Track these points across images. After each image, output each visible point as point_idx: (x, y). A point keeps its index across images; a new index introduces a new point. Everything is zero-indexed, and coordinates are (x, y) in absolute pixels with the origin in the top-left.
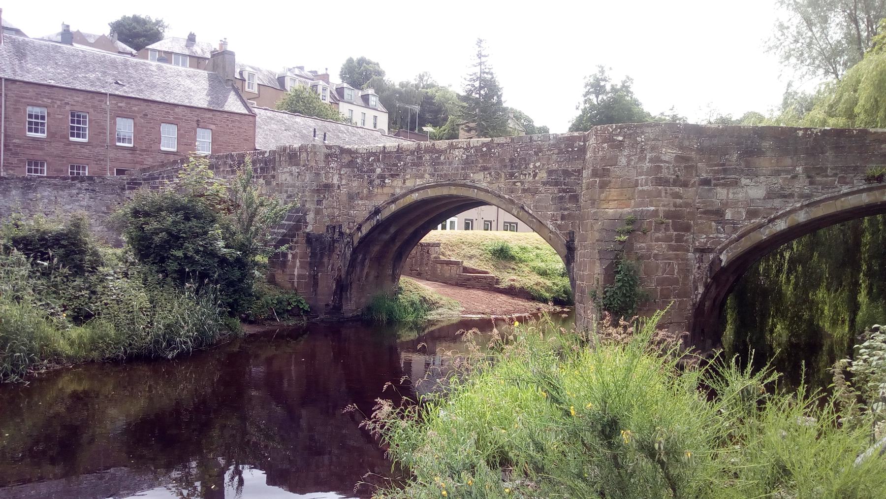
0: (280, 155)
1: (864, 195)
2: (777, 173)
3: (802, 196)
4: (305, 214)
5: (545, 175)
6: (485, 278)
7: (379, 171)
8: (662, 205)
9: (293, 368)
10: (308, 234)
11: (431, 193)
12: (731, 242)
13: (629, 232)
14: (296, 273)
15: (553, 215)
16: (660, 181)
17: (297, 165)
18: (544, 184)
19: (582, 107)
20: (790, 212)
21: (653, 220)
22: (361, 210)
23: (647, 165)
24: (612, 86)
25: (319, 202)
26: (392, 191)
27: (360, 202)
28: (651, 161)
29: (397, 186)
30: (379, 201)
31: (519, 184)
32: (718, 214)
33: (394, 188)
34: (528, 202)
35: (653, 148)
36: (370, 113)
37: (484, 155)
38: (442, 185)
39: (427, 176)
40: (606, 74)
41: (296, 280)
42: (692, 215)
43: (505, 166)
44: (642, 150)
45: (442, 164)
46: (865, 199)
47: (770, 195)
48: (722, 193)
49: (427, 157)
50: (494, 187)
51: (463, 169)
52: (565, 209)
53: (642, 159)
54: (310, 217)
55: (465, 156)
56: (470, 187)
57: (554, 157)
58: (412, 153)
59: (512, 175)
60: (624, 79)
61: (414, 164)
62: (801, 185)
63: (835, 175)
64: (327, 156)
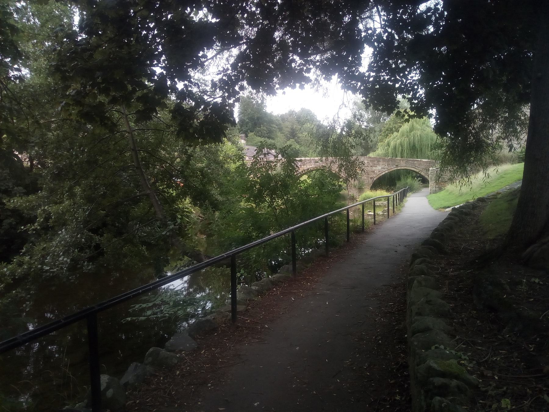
32: (374, 172)
62: (387, 167)
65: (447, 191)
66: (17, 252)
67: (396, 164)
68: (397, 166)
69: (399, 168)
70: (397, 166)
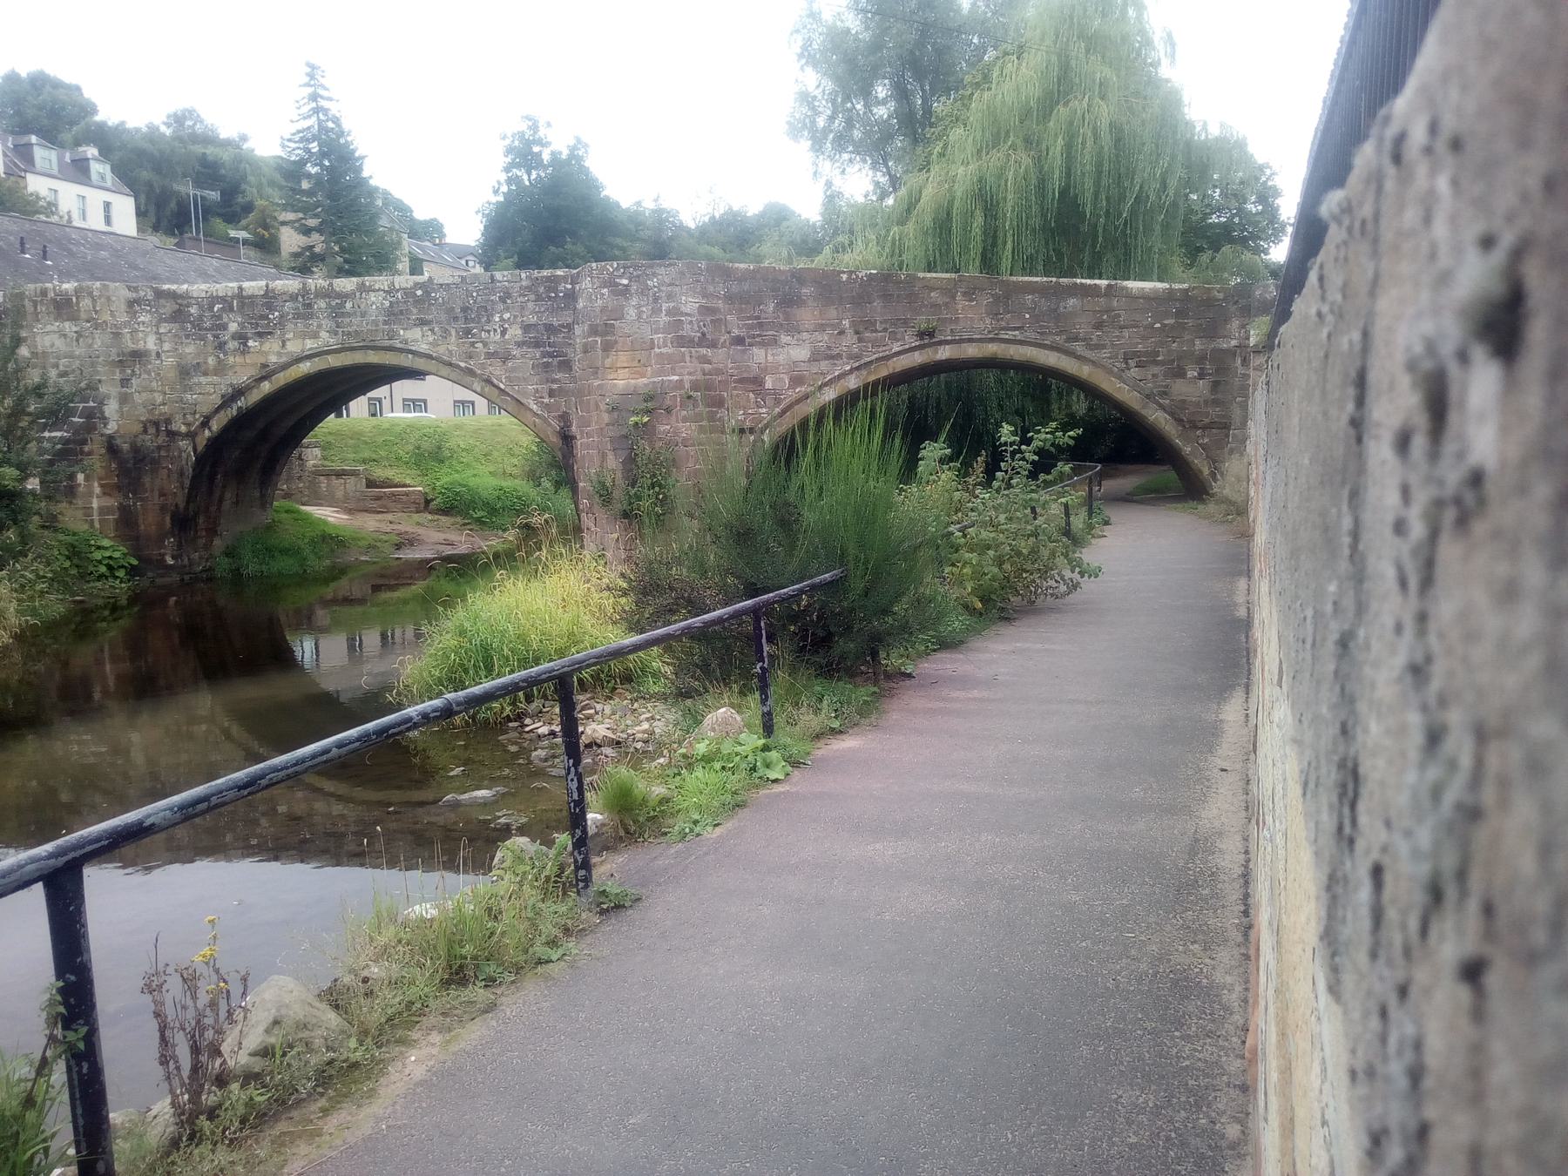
0: (35, 304)
1: (917, 353)
2: (821, 328)
3: (852, 357)
4: (102, 403)
5: (519, 332)
6: (407, 494)
7: (233, 327)
8: (685, 374)
9: (108, 667)
10: (111, 438)
11: (334, 361)
12: (775, 419)
13: (648, 412)
14: (95, 505)
15: (537, 391)
16: (682, 341)
17: (74, 318)
18: (519, 345)
19: (504, 189)
20: (840, 377)
21: (677, 393)
22: (207, 392)
23: (664, 319)
24: (553, 153)
25: (125, 382)
26: (263, 360)
27: (203, 379)
28: (669, 313)
29: (271, 351)
30: (242, 378)
31: (479, 345)
32: (756, 382)
33: (267, 354)
34: (496, 371)
35: (670, 297)
36: (96, 198)
37: (418, 301)
38: (353, 349)
39: (324, 334)
40: (541, 134)
41: (96, 517)
42: (724, 383)
43: (456, 319)
44: (656, 299)
45: (349, 315)
46: (918, 358)
47: (815, 357)
48: (758, 354)
49: (322, 304)
50: (441, 350)
51: (385, 323)
52: (554, 381)
53: (656, 311)
54: (111, 408)
55: (387, 304)
56: (401, 351)
57: (530, 305)
58: (293, 297)
59: (468, 332)
60: (572, 142)
61: (297, 316)
62: (850, 339)
63: (885, 330)
64: (131, 304)
65: (1463, 357)
66: (201, 460)
67: (922, 321)
68: (927, 336)
69: (944, 353)
70: (927, 336)
